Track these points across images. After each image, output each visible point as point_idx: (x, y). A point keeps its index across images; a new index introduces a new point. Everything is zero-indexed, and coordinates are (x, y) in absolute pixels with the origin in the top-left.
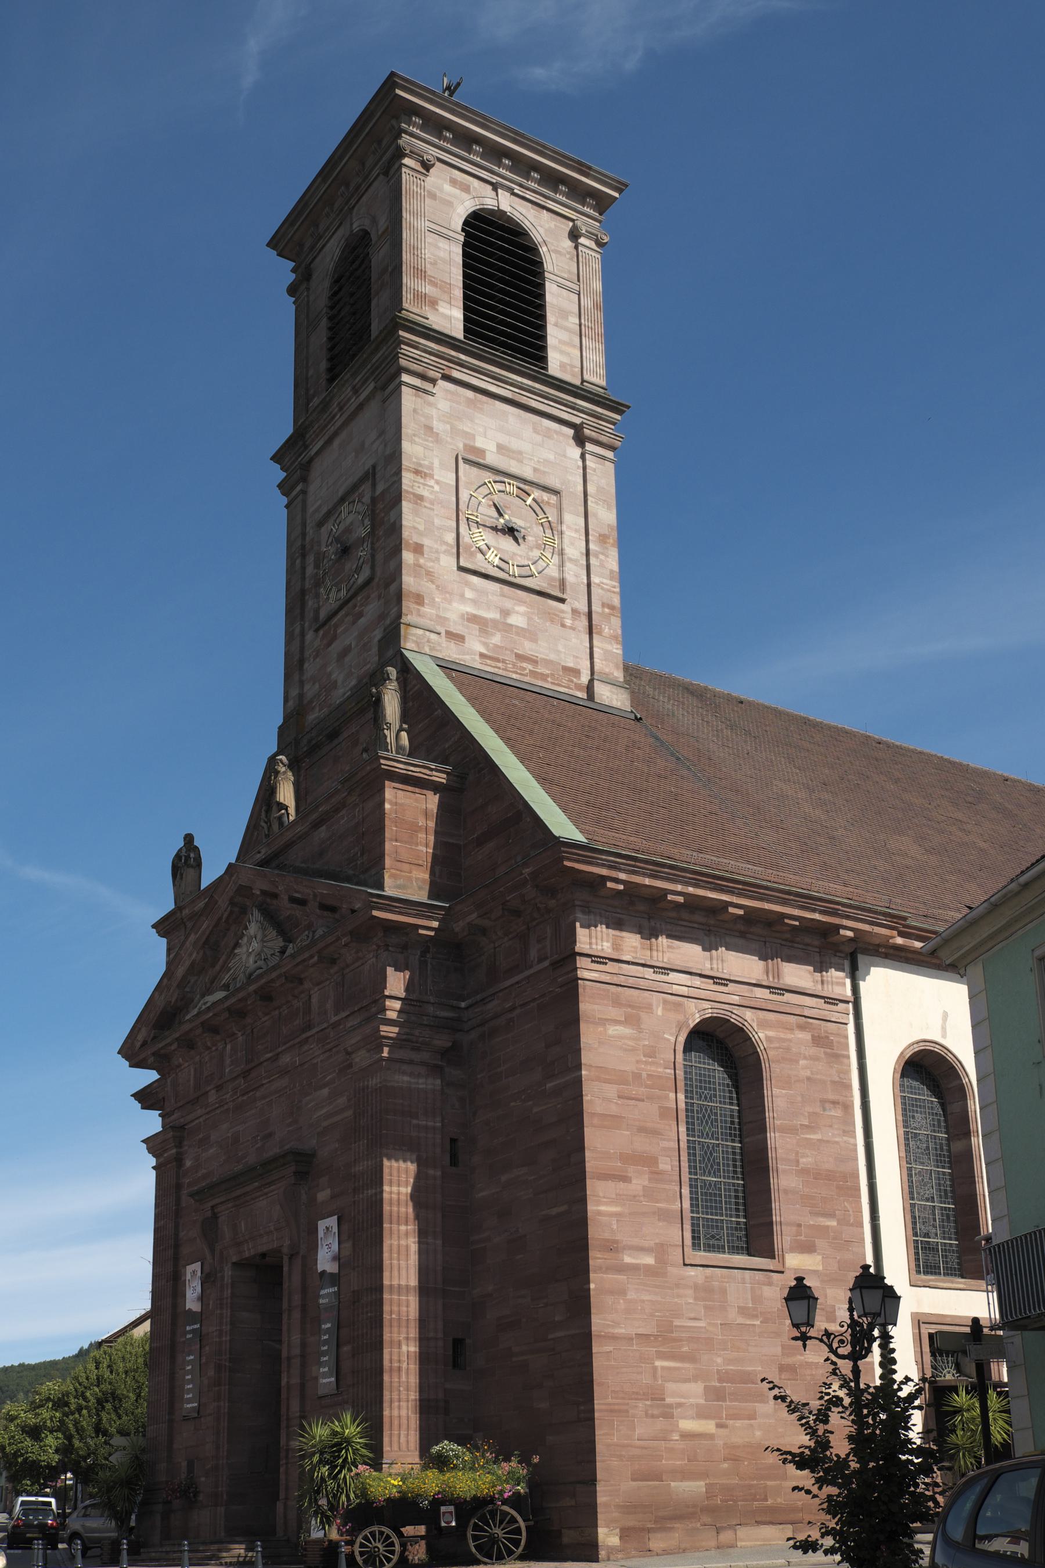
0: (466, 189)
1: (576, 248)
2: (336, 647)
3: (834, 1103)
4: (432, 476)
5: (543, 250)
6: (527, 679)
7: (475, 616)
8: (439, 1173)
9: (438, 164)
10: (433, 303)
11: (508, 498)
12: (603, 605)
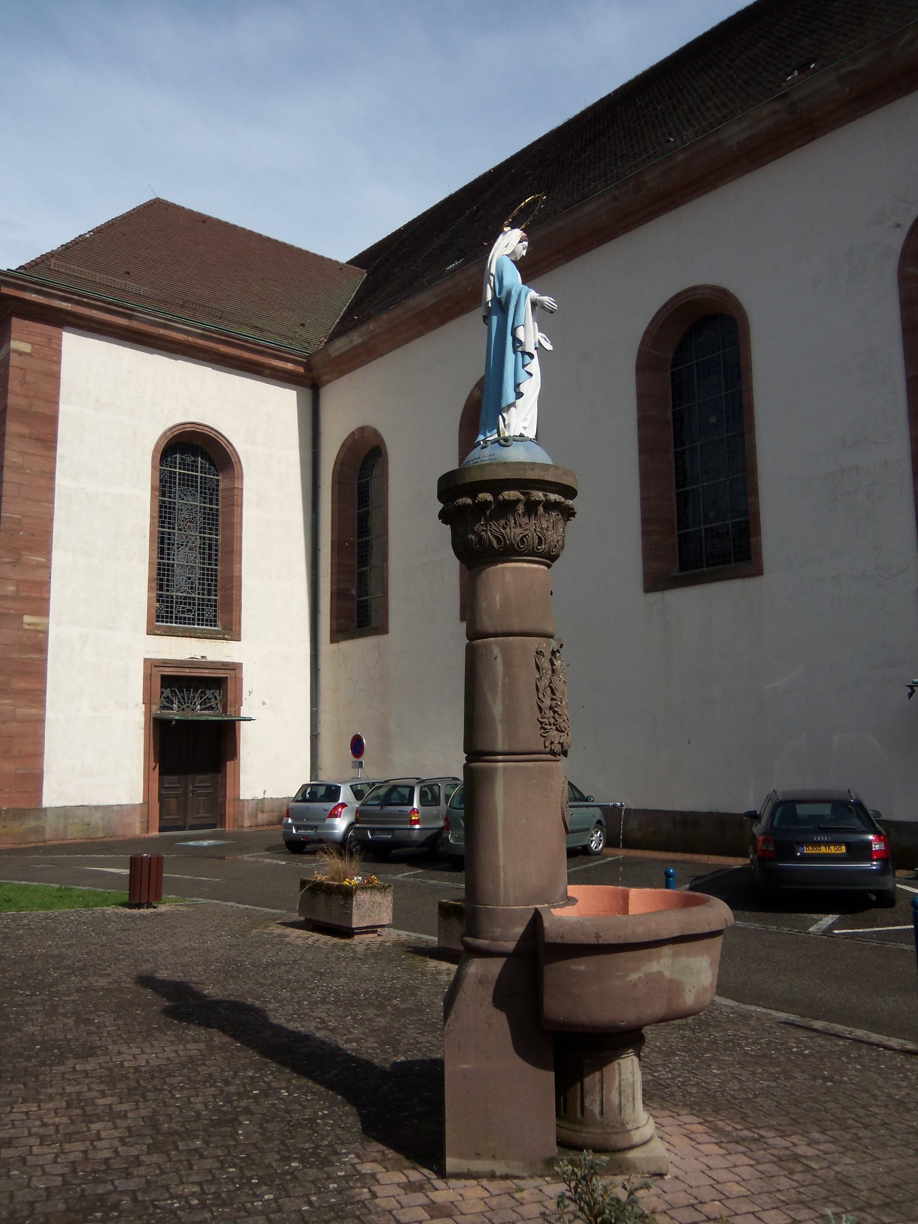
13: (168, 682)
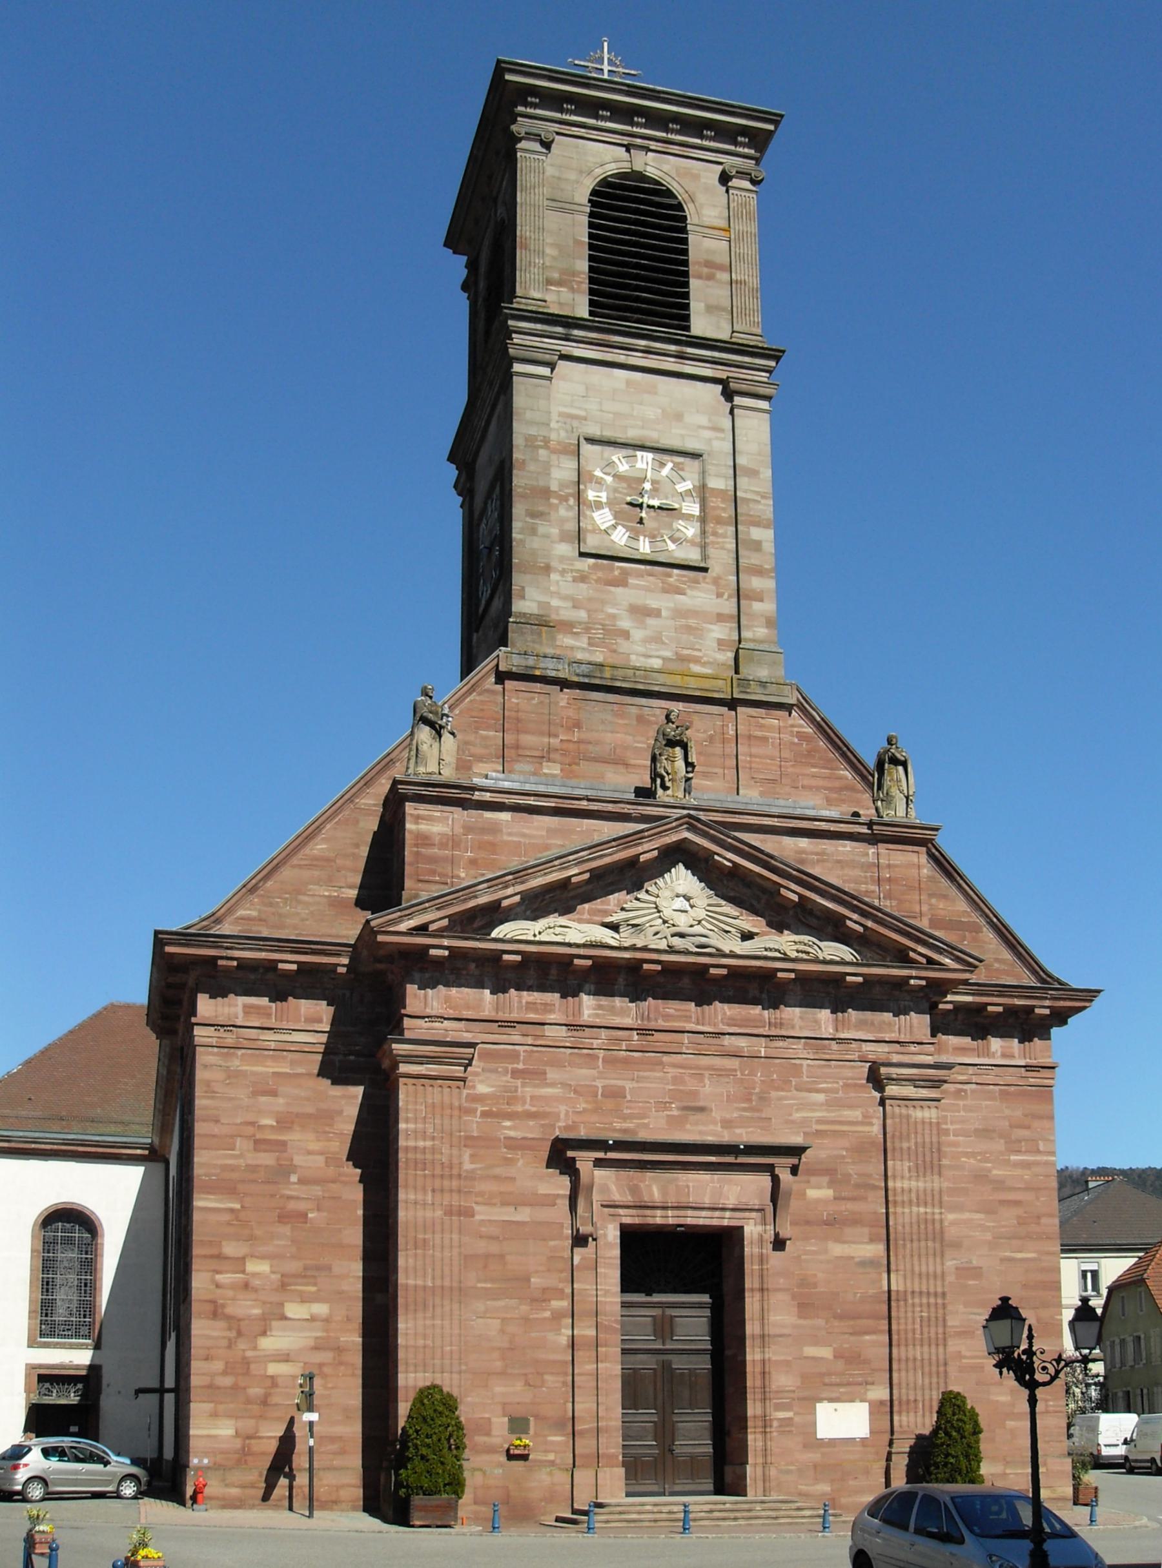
1: (727, 191)
9: (557, 137)
13: (42, 1378)
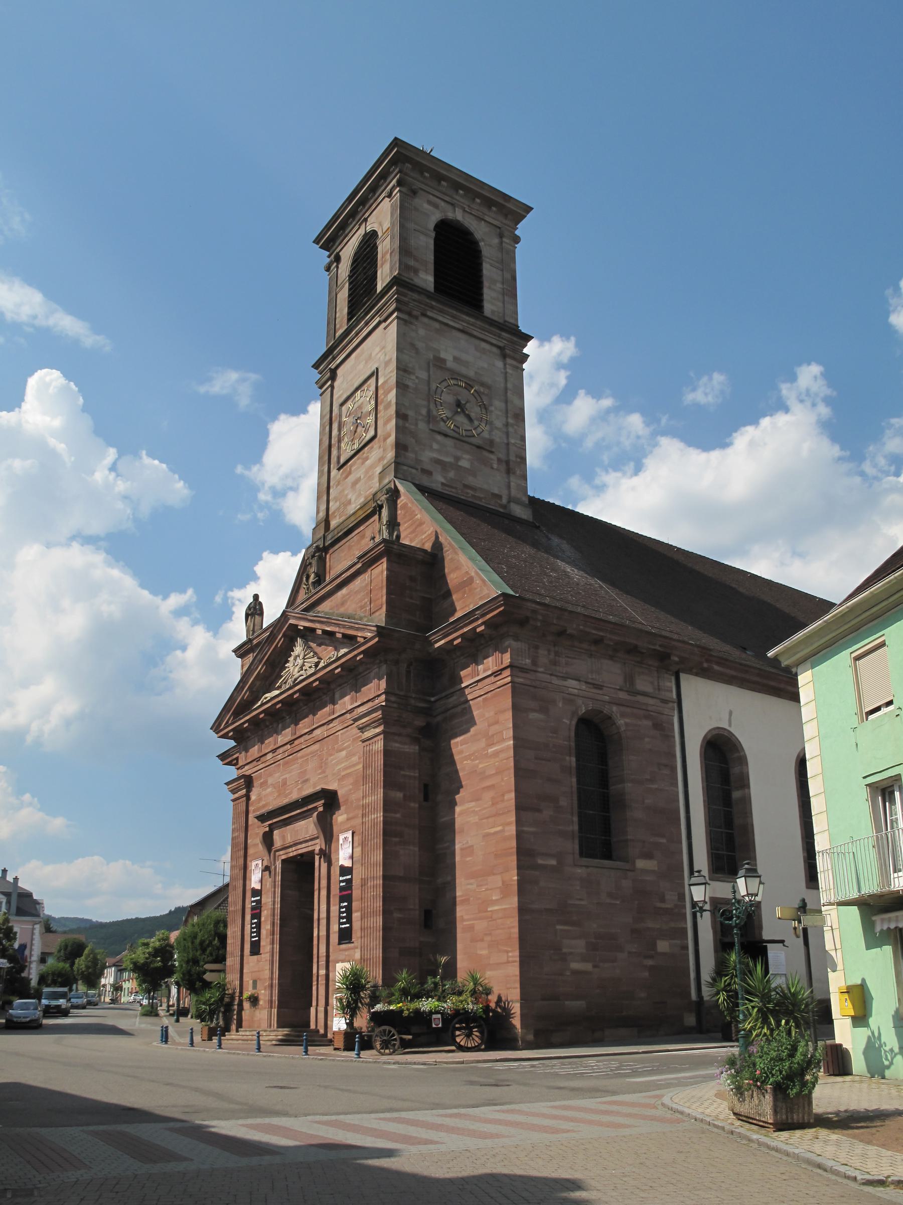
0: (436, 206)
2: (351, 478)
3: (666, 766)
4: (414, 374)
5: (482, 244)
6: (470, 500)
7: (439, 460)
8: (417, 805)
10: (416, 271)
11: (460, 389)
12: (517, 456)
